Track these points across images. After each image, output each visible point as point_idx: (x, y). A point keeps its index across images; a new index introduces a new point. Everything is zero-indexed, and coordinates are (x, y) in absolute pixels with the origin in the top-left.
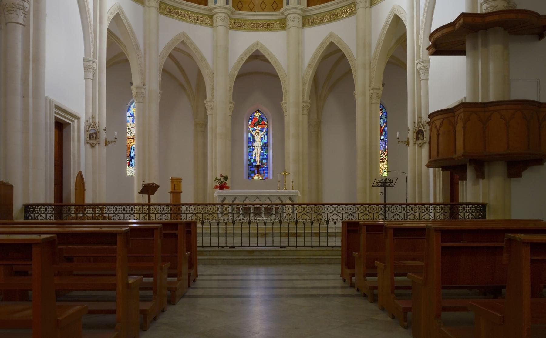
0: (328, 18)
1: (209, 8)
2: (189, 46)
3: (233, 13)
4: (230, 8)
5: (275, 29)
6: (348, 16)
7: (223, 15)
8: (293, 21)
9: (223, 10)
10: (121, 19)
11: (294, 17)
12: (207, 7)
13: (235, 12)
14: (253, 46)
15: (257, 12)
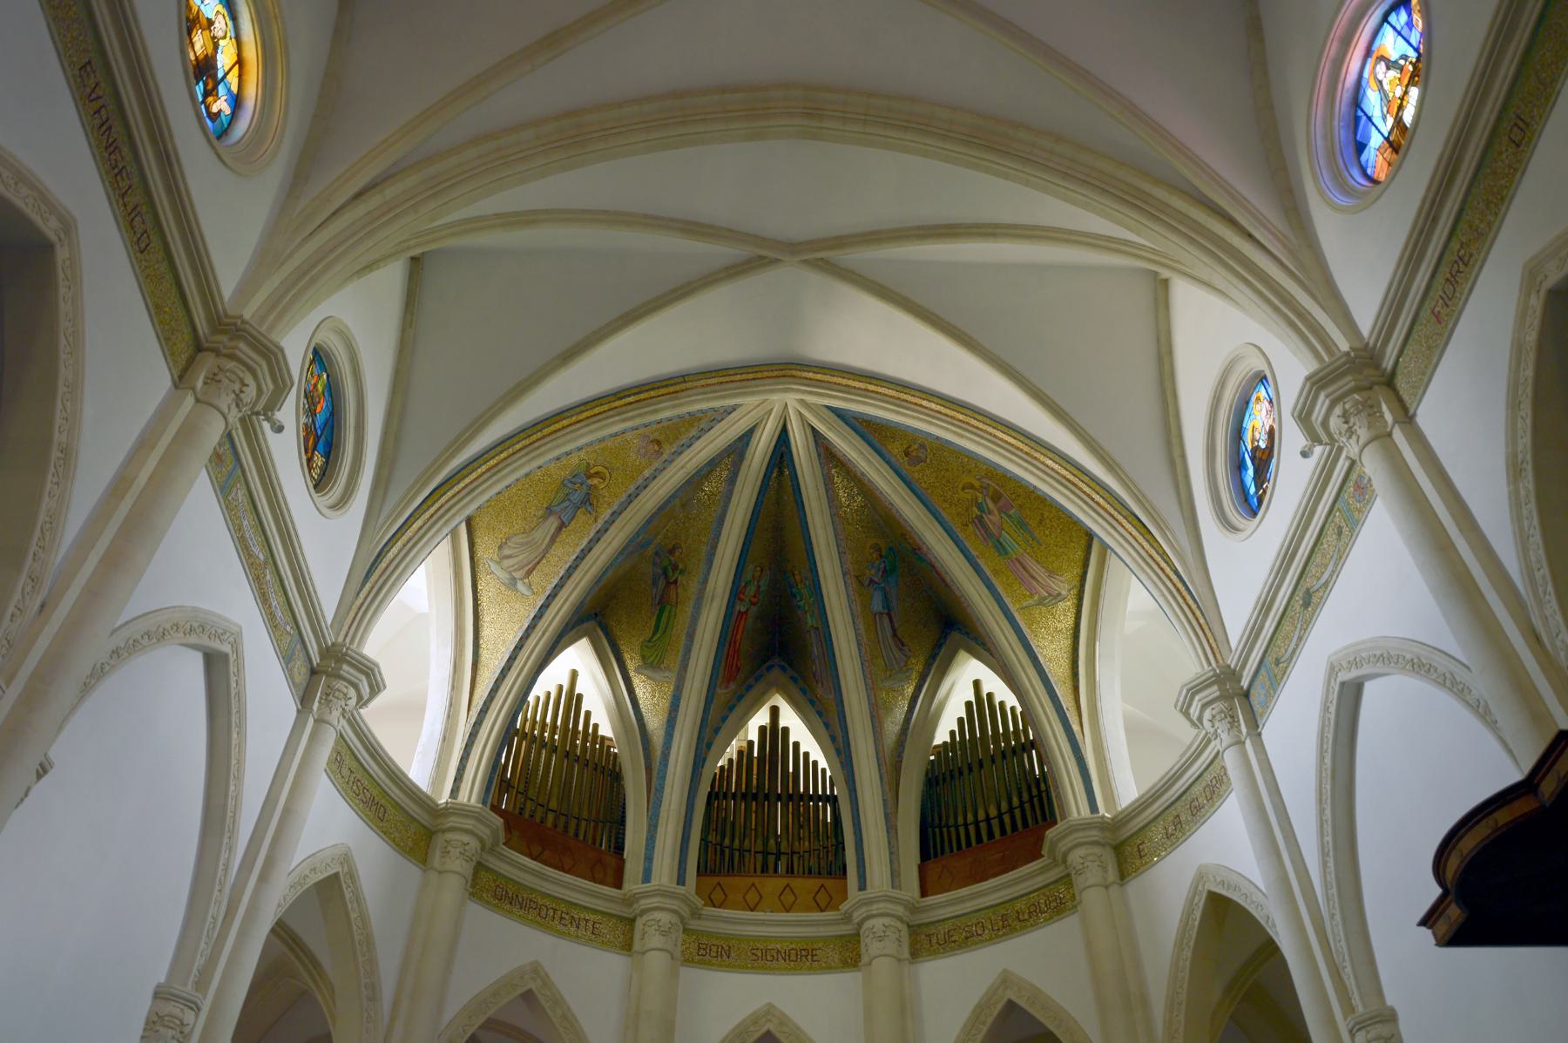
0: (989, 929)
1: (625, 895)
2: (548, 1010)
3: (696, 914)
4: (687, 895)
5: (824, 965)
6: (1051, 918)
7: (665, 918)
8: (881, 939)
9: (668, 901)
10: (343, 896)
11: (885, 927)
12: (618, 891)
13: (703, 912)
14: (755, 1019)
15: (768, 914)
